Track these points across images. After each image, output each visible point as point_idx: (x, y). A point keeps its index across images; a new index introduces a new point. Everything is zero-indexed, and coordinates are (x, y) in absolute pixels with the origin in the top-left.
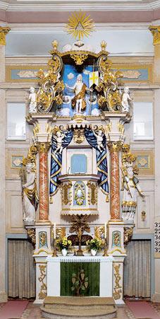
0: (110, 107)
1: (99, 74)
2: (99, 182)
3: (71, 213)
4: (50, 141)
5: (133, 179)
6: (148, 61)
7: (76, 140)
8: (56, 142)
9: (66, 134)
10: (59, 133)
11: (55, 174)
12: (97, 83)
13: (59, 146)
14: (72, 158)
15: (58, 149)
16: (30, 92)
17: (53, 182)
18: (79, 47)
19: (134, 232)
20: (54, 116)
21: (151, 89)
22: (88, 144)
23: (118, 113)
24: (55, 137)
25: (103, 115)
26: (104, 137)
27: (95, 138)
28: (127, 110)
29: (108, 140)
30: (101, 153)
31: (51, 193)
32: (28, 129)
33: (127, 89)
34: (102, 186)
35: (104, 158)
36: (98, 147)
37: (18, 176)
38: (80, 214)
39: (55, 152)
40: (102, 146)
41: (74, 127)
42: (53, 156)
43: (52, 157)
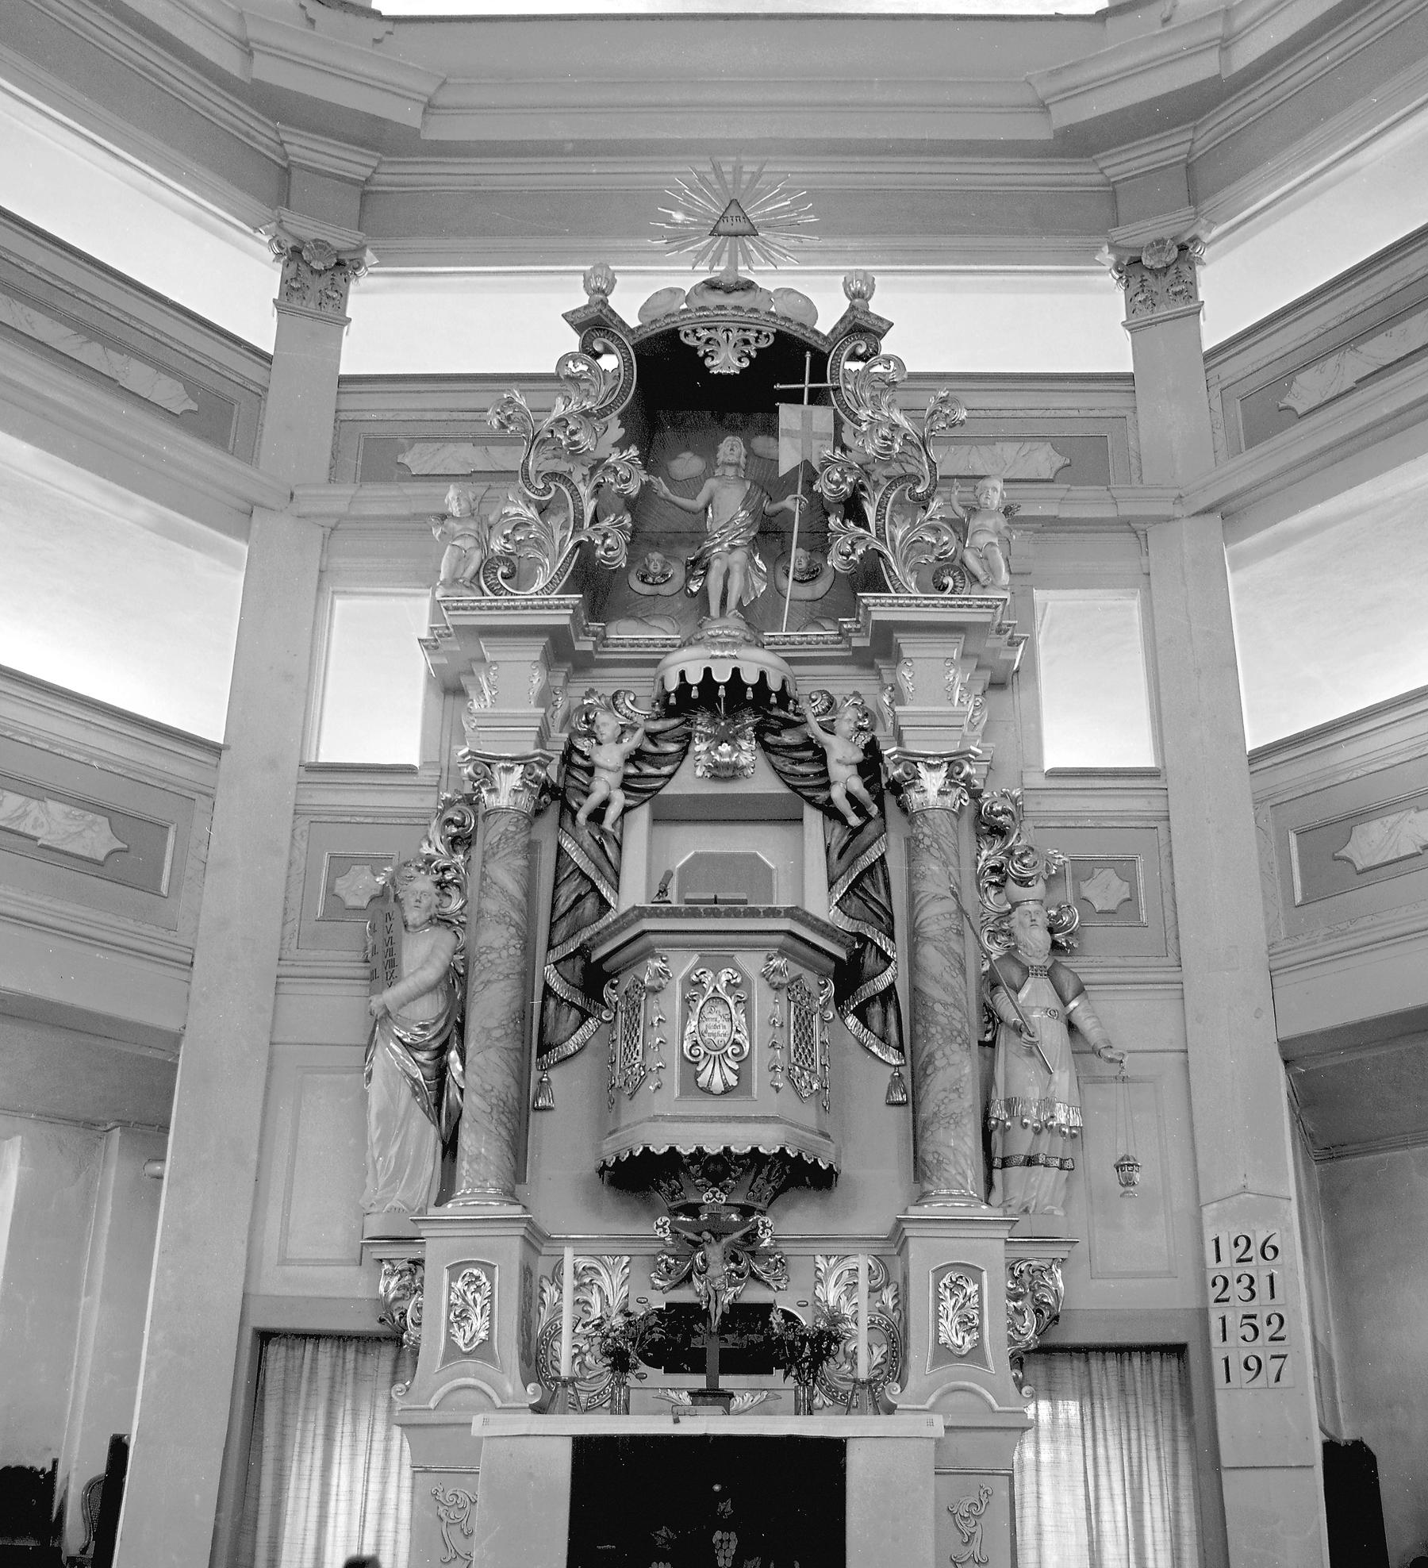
1: (838, 424)
10: (607, 724)
13: (605, 784)
17: (557, 986)
22: (777, 788)
31: (544, 1048)
34: (861, 1013)
35: (873, 854)
36: (837, 793)
40: (857, 785)
42: (568, 845)
43: (560, 851)
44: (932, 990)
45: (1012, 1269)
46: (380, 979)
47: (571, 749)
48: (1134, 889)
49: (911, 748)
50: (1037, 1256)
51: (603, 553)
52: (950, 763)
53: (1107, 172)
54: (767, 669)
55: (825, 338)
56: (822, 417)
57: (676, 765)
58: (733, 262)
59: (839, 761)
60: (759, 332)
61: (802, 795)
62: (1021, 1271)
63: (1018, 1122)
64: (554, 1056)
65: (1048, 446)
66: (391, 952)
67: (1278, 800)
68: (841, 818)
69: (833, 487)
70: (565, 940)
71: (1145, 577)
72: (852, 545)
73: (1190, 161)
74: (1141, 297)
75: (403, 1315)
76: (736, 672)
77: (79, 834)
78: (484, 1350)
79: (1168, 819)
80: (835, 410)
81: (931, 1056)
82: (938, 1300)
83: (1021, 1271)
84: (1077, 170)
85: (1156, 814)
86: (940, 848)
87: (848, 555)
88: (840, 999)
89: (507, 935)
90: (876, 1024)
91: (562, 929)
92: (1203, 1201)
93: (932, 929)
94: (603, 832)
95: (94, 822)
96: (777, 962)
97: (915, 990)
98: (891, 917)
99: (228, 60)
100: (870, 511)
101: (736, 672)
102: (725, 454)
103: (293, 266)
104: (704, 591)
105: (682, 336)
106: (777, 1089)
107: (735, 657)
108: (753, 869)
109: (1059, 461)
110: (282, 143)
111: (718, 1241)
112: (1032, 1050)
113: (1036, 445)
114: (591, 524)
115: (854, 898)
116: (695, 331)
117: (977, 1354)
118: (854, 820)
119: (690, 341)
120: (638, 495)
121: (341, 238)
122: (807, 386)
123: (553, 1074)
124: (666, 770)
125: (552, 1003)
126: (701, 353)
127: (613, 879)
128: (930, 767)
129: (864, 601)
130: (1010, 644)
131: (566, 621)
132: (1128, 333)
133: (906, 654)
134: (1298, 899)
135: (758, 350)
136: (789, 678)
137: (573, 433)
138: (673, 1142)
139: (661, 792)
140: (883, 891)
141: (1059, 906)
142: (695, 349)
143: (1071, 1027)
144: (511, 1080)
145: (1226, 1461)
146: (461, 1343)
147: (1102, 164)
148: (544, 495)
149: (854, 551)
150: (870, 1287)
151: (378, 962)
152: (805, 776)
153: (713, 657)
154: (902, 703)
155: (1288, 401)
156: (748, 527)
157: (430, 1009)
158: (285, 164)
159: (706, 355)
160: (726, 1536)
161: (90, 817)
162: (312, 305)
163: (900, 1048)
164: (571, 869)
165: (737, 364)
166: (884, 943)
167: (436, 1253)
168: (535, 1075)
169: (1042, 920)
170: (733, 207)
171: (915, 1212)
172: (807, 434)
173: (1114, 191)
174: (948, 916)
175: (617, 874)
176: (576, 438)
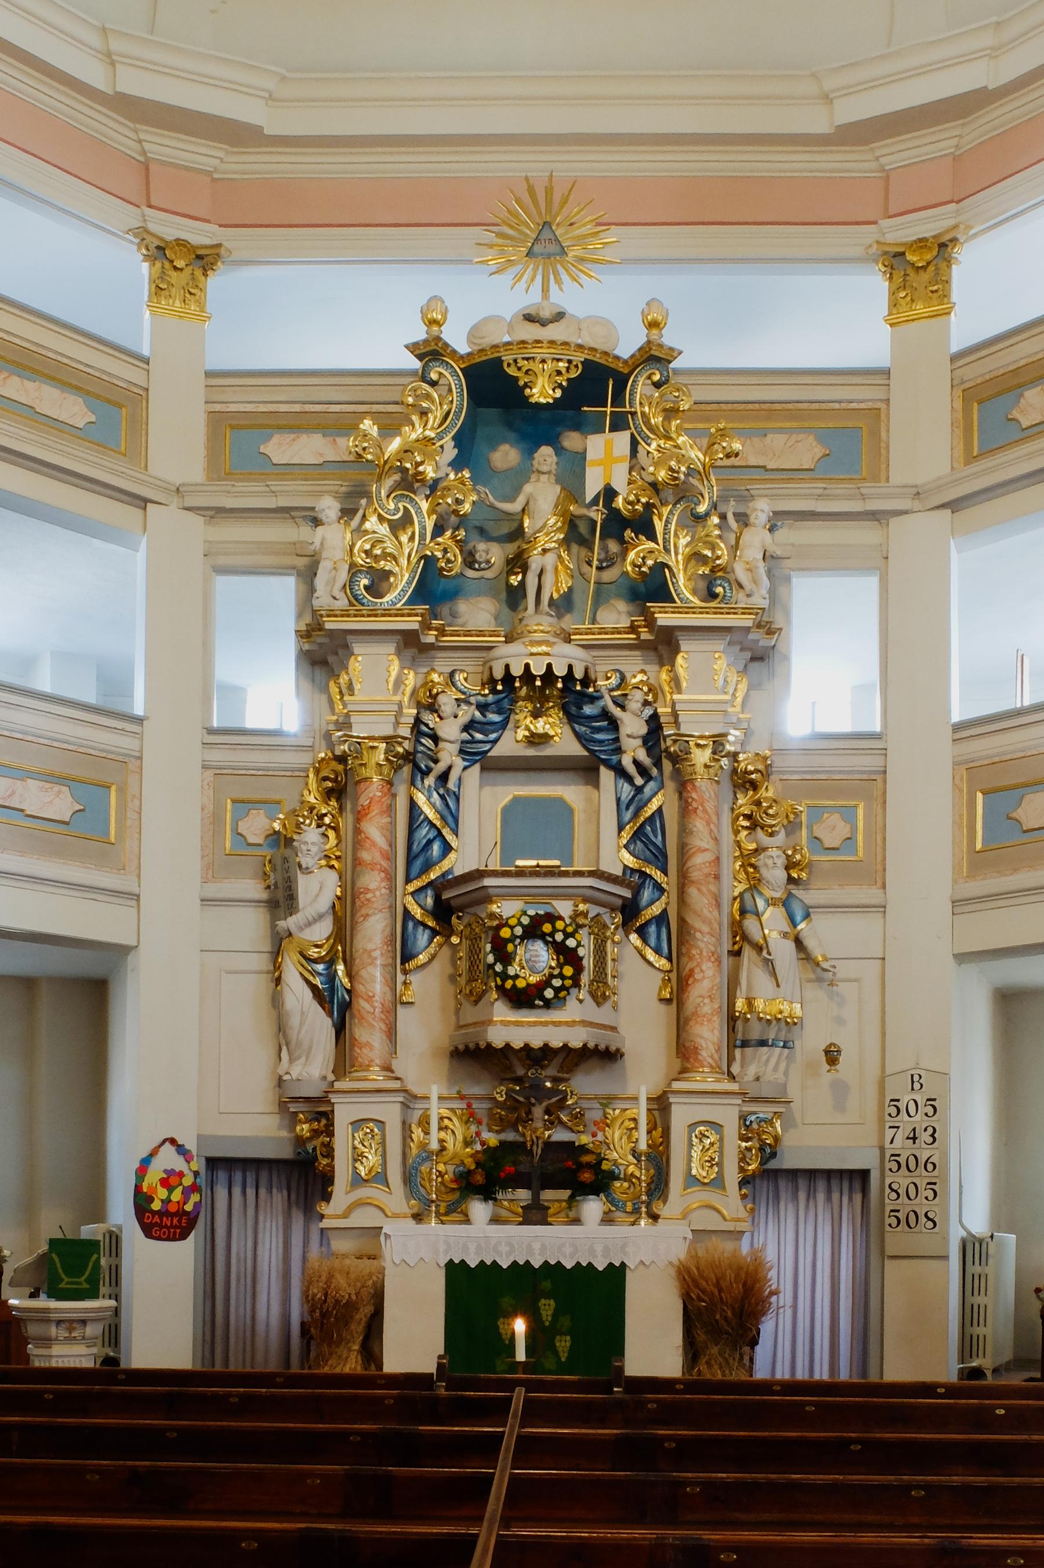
0: (682, 584)
1: (634, 444)
2: (629, 911)
3: (497, 1037)
4: (405, 731)
5: (786, 903)
6: (865, 394)
7: (522, 733)
8: (436, 739)
9: (482, 707)
10: (447, 702)
11: (424, 880)
12: (620, 484)
13: (449, 755)
14: (506, 811)
15: (441, 767)
16: (316, 522)
17: (417, 912)
18: (544, 323)
19: (790, 1140)
20: (426, 626)
21: (875, 516)
23: (717, 611)
24: (429, 718)
25: (650, 622)
26: (654, 722)
27: (614, 725)
28: (761, 599)
29: (667, 731)
30: (639, 790)
32: (306, 685)
33: (761, 509)
34: (642, 932)
36: (627, 761)
37: (254, 889)
38: (536, 1043)
39: (430, 781)
40: (642, 755)
41: (517, 671)
42: (421, 799)
43: (413, 805)
44: (693, 921)
45: (745, 1120)
46: (282, 908)
47: (418, 721)
48: (854, 829)
49: (684, 730)
50: (765, 1111)
51: (443, 565)
52: (714, 742)
53: (883, 160)
54: (574, 662)
55: (625, 362)
56: (622, 440)
57: (500, 732)
58: (545, 291)
59: (629, 736)
60: (570, 362)
61: (599, 758)
62: (751, 1122)
63: (755, 1015)
64: (412, 964)
65: (811, 438)
66: (290, 888)
67: (972, 765)
68: (630, 779)
69: (630, 507)
70: (419, 876)
71: (884, 560)
72: (644, 558)
73: (957, 153)
74: (902, 294)
75: (314, 1149)
76: (549, 666)
77: (51, 802)
78: (381, 1178)
79: (885, 772)
80: (632, 435)
81: (692, 971)
82: (691, 1145)
83: (751, 1122)
84: (850, 157)
85: (876, 769)
86: (705, 811)
87: (640, 567)
88: (625, 924)
89: (379, 879)
90: (653, 941)
91: (418, 864)
92: (888, 1072)
93: (695, 875)
94: (448, 791)
95: (59, 792)
96: (582, 907)
97: (682, 921)
98: (665, 856)
99: (94, 75)
100: (659, 526)
101: (549, 666)
102: (539, 463)
103: (158, 265)
104: (522, 584)
105: (505, 365)
106: (581, 1001)
107: (548, 654)
108: (563, 810)
109: (819, 451)
110: (140, 141)
111: (540, 1103)
112: (770, 966)
113: (801, 437)
114: (433, 538)
115: (638, 842)
116: (515, 361)
117: (718, 1183)
118: (639, 781)
119: (512, 371)
120: (604, 1171)
121: (199, 235)
122: (609, 410)
123: (411, 978)
124: (493, 736)
125: (411, 925)
126: (521, 383)
127: (453, 825)
128: (698, 745)
129: (652, 609)
130: (767, 634)
131: (416, 626)
132: (888, 326)
133: (683, 647)
134: (979, 846)
135: (568, 380)
136: (590, 665)
137: (418, 464)
138: (508, 1039)
139: (489, 754)
140: (660, 837)
141: (794, 847)
142: (517, 379)
143: (799, 943)
144: (388, 988)
145: (889, 1252)
146: (363, 1174)
147: (878, 153)
148: (394, 514)
149: (644, 563)
150: (619, 742)
151: (280, 895)
152: (601, 742)
153: (532, 654)
154: (680, 692)
155: (1015, 414)
156: (559, 530)
157: (322, 931)
158: (142, 159)
159: (526, 385)
160: (547, 1302)
161: (56, 788)
162: (178, 304)
163: (669, 959)
164: (422, 817)
165: (551, 392)
166: (658, 875)
167: (344, 1114)
168: (400, 978)
169: (781, 861)
170: (546, 230)
171: (677, 1085)
172: (609, 460)
173: (888, 177)
174: (707, 865)
175: (456, 820)
176: (421, 469)
